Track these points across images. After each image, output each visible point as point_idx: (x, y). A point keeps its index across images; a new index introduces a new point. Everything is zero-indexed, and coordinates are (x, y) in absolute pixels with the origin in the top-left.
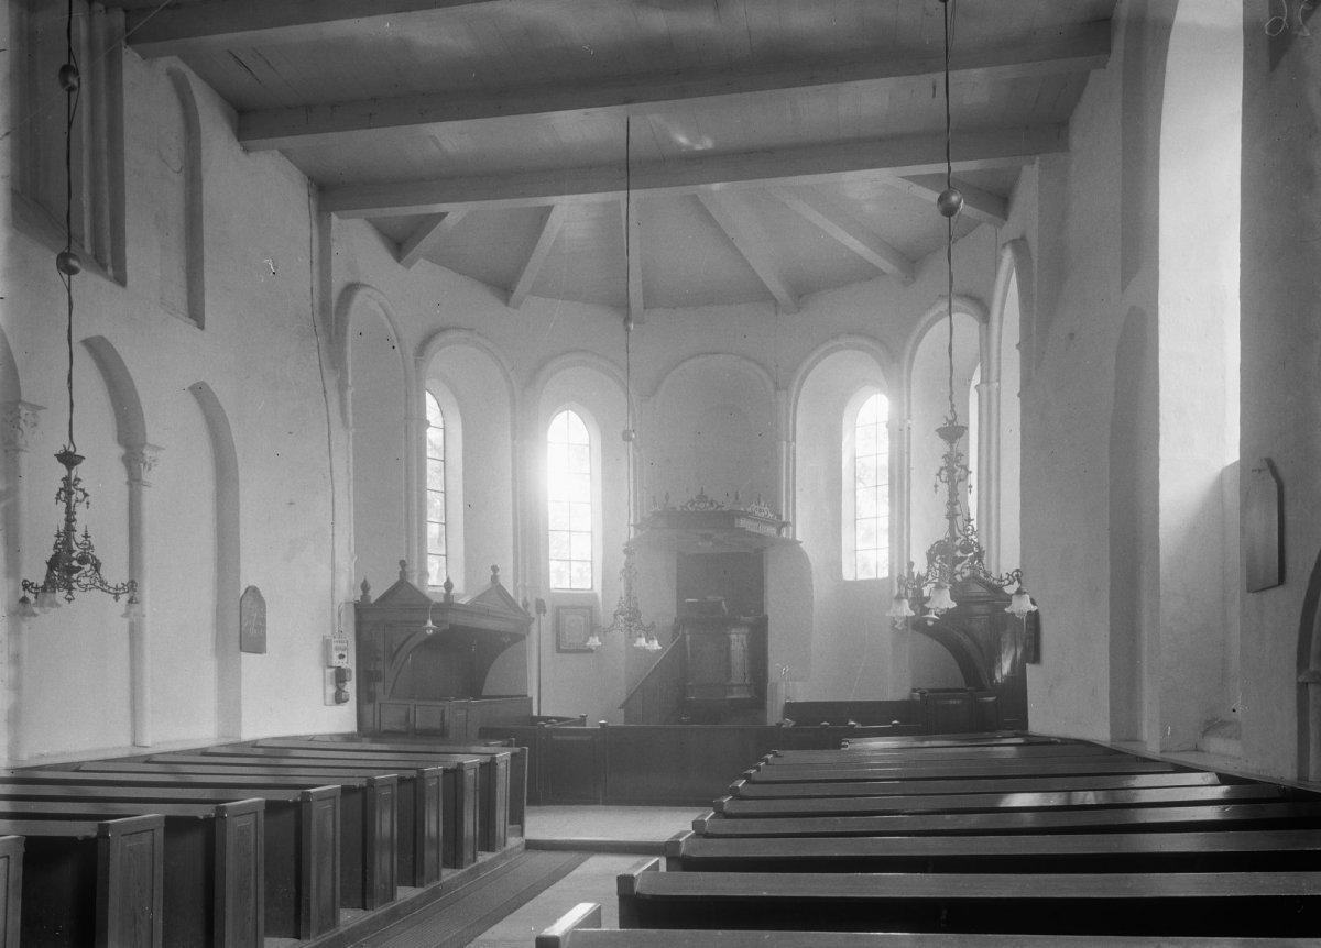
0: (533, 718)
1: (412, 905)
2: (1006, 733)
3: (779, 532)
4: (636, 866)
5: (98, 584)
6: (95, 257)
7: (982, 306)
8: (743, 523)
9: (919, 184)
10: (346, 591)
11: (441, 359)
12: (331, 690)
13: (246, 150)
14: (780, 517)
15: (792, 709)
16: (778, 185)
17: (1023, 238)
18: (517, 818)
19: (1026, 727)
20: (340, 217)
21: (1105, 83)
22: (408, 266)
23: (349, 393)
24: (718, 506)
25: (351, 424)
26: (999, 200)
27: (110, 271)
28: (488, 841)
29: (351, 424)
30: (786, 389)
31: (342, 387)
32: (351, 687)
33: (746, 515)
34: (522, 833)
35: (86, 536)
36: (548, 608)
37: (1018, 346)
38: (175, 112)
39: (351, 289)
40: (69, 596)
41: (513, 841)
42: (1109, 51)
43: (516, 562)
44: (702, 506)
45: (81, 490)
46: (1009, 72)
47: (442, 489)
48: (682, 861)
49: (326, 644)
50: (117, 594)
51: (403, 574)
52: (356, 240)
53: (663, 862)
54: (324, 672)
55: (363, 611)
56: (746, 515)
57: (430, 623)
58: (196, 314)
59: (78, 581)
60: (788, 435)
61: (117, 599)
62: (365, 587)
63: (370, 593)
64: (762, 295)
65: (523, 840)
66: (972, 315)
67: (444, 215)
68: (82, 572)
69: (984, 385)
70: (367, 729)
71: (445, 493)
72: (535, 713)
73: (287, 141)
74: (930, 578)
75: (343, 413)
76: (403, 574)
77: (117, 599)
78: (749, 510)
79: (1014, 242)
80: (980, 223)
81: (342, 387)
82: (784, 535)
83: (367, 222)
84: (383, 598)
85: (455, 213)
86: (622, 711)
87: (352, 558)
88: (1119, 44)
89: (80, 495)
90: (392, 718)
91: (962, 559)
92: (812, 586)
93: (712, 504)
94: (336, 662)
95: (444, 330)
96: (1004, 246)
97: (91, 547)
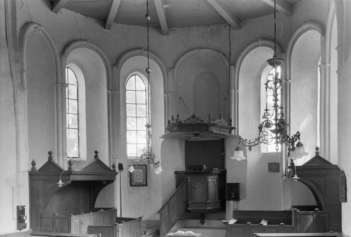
0: (118, 218)
3: (230, 132)
10: (26, 167)
14: (231, 125)
22: (56, 12)
23: (25, 74)
24: (201, 121)
25: (26, 88)
29: (26, 88)
37: (336, 48)
44: (194, 120)
47: (77, 114)
51: (50, 158)
56: (214, 125)
57: (60, 182)
60: (235, 86)
63: (36, 166)
71: (78, 114)
72: (119, 215)
74: (261, 140)
78: (216, 122)
81: (22, 71)
82: (233, 133)
86: (159, 214)
93: (198, 120)
95: (74, 41)
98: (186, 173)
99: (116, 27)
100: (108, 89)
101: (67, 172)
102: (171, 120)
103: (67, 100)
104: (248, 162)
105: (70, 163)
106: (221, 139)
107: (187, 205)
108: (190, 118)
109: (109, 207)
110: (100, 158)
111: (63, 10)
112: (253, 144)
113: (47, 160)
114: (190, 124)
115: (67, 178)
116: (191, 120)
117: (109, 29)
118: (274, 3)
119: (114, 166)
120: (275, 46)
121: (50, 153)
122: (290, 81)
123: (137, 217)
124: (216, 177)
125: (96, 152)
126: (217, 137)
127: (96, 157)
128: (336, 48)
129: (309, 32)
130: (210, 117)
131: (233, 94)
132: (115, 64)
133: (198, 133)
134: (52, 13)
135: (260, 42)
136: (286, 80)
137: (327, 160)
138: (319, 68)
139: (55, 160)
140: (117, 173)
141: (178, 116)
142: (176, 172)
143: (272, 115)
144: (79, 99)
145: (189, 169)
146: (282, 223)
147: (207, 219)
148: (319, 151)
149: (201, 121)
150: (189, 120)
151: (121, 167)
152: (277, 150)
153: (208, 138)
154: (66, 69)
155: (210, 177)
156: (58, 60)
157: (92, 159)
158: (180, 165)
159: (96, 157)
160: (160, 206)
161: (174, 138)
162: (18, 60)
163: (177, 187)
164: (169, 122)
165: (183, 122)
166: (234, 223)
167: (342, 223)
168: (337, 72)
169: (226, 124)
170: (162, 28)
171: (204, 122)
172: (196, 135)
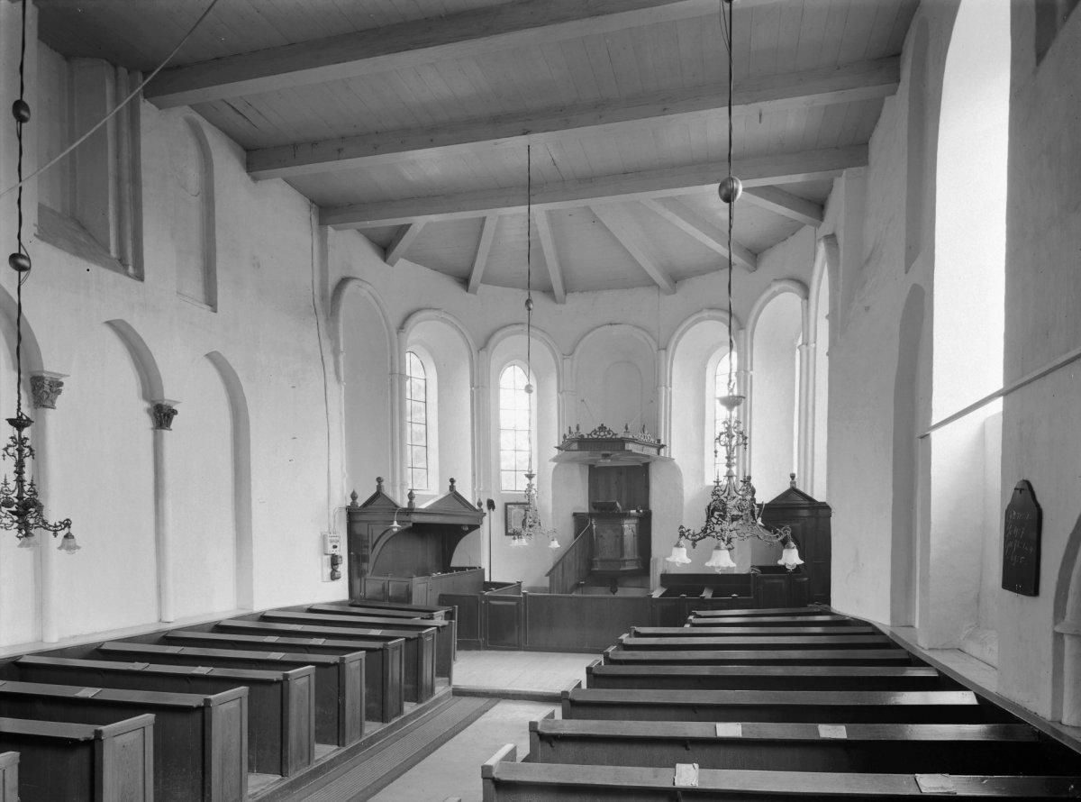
0: (485, 583)
1: (331, 764)
4: (538, 713)
5: (41, 523)
7: (805, 288)
8: (630, 446)
9: (752, 193)
10: (341, 500)
11: (419, 331)
12: (329, 570)
13: (255, 179)
14: (659, 441)
15: (666, 579)
16: (648, 198)
18: (445, 670)
20: (335, 229)
21: (897, 109)
22: (392, 265)
23: (341, 358)
26: (816, 205)
27: (131, 270)
28: (418, 691)
30: (665, 349)
31: (336, 352)
32: (343, 568)
33: (633, 441)
34: (450, 683)
35: (32, 485)
36: (499, 505)
38: (193, 151)
39: (344, 281)
41: (441, 689)
42: (898, 81)
44: (602, 434)
45: (28, 447)
46: (824, 99)
48: (572, 704)
49: (324, 538)
51: (379, 487)
52: (350, 247)
53: (558, 711)
54: (322, 559)
55: (353, 514)
57: (395, 524)
58: (212, 303)
61: (55, 535)
63: (357, 501)
64: (651, 283)
65: (450, 689)
66: (796, 293)
70: (355, 600)
72: (487, 579)
73: (288, 171)
74: (708, 531)
76: (379, 487)
77: (55, 535)
79: (827, 237)
80: (805, 224)
83: (357, 233)
84: (365, 505)
85: (419, 222)
86: (548, 578)
87: (345, 476)
88: (906, 73)
90: (372, 586)
94: (331, 550)
97: (35, 493)
98: (591, 515)
99: (402, 264)
100: (472, 385)
101: (405, 509)
102: (567, 433)
104: (685, 498)
105: (411, 496)
107: (590, 563)
109: (473, 565)
110: (458, 489)
111: (401, 261)
112: (698, 537)
113: (374, 491)
115: (405, 518)
117: (392, 265)
118: (728, 251)
119: (480, 504)
120: (731, 341)
121: (379, 480)
124: (635, 521)
125: (452, 481)
126: (637, 460)
127: (452, 488)
129: (781, 296)
130: (627, 428)
132: (485, 347)
133: (609, 452)
134: (387, 266)
135: (705, 314)
136: (746, 371)
137: (809, 494)
138: (798, 352)
139: (387, 491)
141: (578, 428)
142: (575, 515)
143: (14, 491)
144: (428, 401)
145: (595, 508)
147: (621, 586)
150: (595, 434)
151: (491, 504)
152: (731, 390)
153: (625, 462)
154: (408, 355)
155: (626, 522)
156: (394, 331)
157: (447, 490)
158: (580, 501)
159: (452, 488)
160: (551, 566)
161: (573, 460)
162: (333, 335)
163: (576, 537)
164: (565, 437)
165: (586, 436)
167: (934, 393)
168: (828, 354)
170: (555, 292)
171: (619, 436)
172: (606, 456)
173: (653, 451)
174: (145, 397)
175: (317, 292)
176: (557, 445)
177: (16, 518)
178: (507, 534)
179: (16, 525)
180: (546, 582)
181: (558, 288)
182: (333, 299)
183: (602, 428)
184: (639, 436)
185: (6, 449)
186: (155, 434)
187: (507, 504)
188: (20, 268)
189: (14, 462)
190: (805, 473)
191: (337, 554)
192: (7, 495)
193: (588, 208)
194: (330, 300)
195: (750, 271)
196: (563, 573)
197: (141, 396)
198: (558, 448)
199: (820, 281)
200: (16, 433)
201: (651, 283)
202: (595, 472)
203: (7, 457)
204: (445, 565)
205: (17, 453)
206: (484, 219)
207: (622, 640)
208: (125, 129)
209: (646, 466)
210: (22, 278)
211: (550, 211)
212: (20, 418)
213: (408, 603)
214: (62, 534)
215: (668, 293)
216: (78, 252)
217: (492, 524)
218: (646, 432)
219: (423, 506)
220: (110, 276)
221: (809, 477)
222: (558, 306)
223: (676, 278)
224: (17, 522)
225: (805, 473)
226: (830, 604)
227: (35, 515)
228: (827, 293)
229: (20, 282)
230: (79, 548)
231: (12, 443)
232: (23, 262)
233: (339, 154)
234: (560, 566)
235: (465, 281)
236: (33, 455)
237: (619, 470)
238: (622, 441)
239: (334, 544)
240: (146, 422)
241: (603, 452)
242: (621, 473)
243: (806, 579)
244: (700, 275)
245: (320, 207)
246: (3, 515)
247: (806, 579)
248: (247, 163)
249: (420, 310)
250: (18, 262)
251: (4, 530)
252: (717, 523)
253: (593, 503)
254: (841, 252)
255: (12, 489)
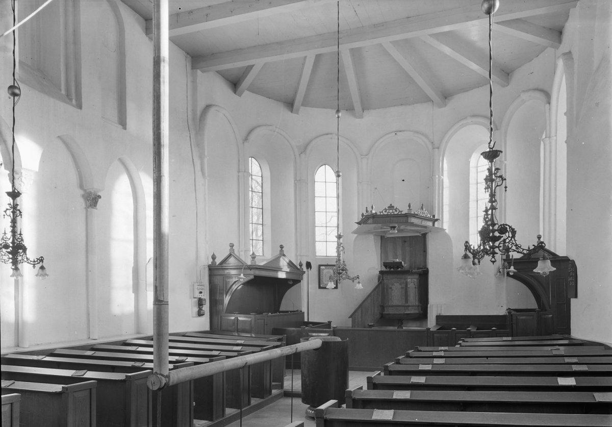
2: (558, 336)
3: (434, 225)
5: (25, 260)
6: (67, 96)
8: (413, 220)
9: (502, 25)
12: (196, 309)
14: (434, 216)
15: (439, 318)
17: (570, 52)
19: (569, 333)
20: (203, 72)
23: (206, 160)
29: (206, 175)
30: (438, 148)
31: (201, 157)
32: (206, 308)
37: (565, 114)
39: (208, 107)
40: (493, 260)
43: (296, 241)
44: (391, 211)
50: (34, 264)
58: (123, 123)
59: (498, 247)
62: (214, 257)
67: (250, 68)
68: (502, 239)
69: (548, 139)
72: (306, 320)
75: (202, 170)
79: (564, 54)
80: (547, 47)
81: (201, 157)
85: (258, 63)
89: (18, 212)
91: (499, 238)
92: (452, 253)
93: (396, 211)
94: (198, 295)
96: (559, 57)
103: (250, 193)
106: (422, 234)
108: (387, 208)
114: (387, 215)
115: (249, 272)
116: (388, 211)
117: (240, 96)
119: (301, 265)
122: (506, 162)
123: (325, 321)
128: (565, 114)
131: (437, 197)
135: (469, 120)
137: (552, 250)
140: (305, 272)
143: (10, 239)
145: (386, 267)
146: (494, 328)
148: (542, 240)
149: (400, 211)
151: (309, 265)
155: (409, 277)
161: (369, 232)
162: (199, 145)
164: (363, 215)
166: (438, 330)
169: (428, 215)
171: (403, 213)
173: (430, 224)
174: (81, 186)
175: (190, 117)
176: (357, 221)
177: (11, 256)
178: (320, 287)
179: (11, 260)
180: (349, 324)
181: (357, 106)
182: (200, 120)
183: (391, 207)
184: (419, 212)
185: (5, 212)
186: (87, 211)
187: (320, 266)
188: (14, 95)
189: (10, 220)
190: (550, 233)
191: (202, 297)
192: (6, 241)
193: (381, 45)
194: (198, 120)
195: (504, 86)
196: (362, 316)
197: (79, 186)
198: (357, 223)
199: (559, 89)
200: (11, 201)
201: (428, 100)
202: (384, 241)
203: (6, 216)
204: (275, 307)
205: (12, 214)
206: (306, 57)
207: (409, 353)
208: (70, 9)
209: (424, 235)
210: (15, 101)
211: (352, 49)
212: (14, 191)
213: (223, 417)
214: (38, 266)
215: (440, 107)
216: (43, 91)
217: (309, 281)
218: (424, 209)
219: (262, 264)
220: (62, 106)
221: (553, 228)
222: (357, 120)
223: (446, 96)
224: (11, 258)
225: (550, 233)
226: (570, 334)
227: (21, 255)
228: (565, 96)
229: (14, 104)
230: (47, 275)
231: (9, 208)
232: (17, 91)
233: (207, 18)
234: (360, 310)
235: (290, 104)
236: (21, 215)
237: (404, 240)
238: (407, 216)
239: (200, 291)
240: (81, 203)
241: (391, 225)
242: (405, 242)
243: (550, 316)
244: (464, 92)
245: (192, 57)
246: (3, 254)
247: (550, 316)
248: (146, 29)
249: (259, 126)
250: (14, 91)
251: (345, 250)
252: (5, 255)
253: (384, 263)
254: (576, 66)
255: (9, 237)
